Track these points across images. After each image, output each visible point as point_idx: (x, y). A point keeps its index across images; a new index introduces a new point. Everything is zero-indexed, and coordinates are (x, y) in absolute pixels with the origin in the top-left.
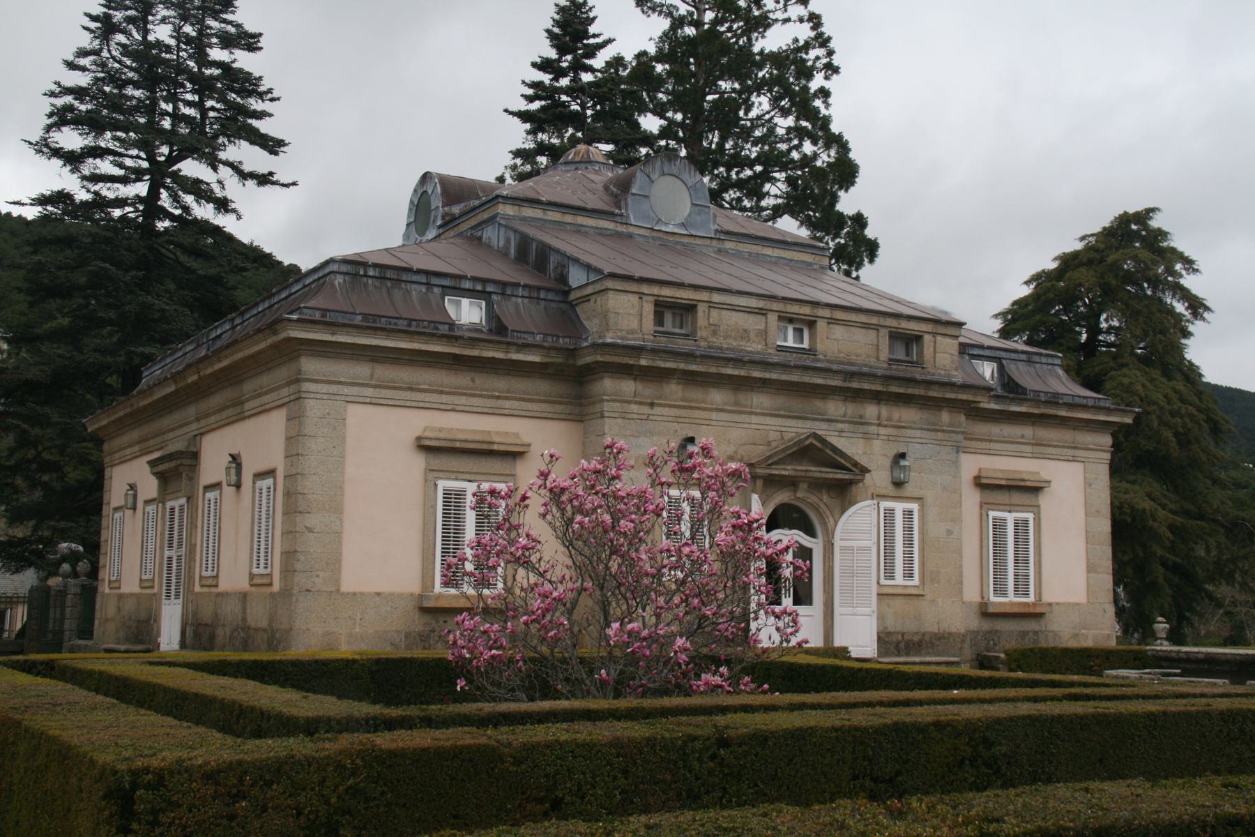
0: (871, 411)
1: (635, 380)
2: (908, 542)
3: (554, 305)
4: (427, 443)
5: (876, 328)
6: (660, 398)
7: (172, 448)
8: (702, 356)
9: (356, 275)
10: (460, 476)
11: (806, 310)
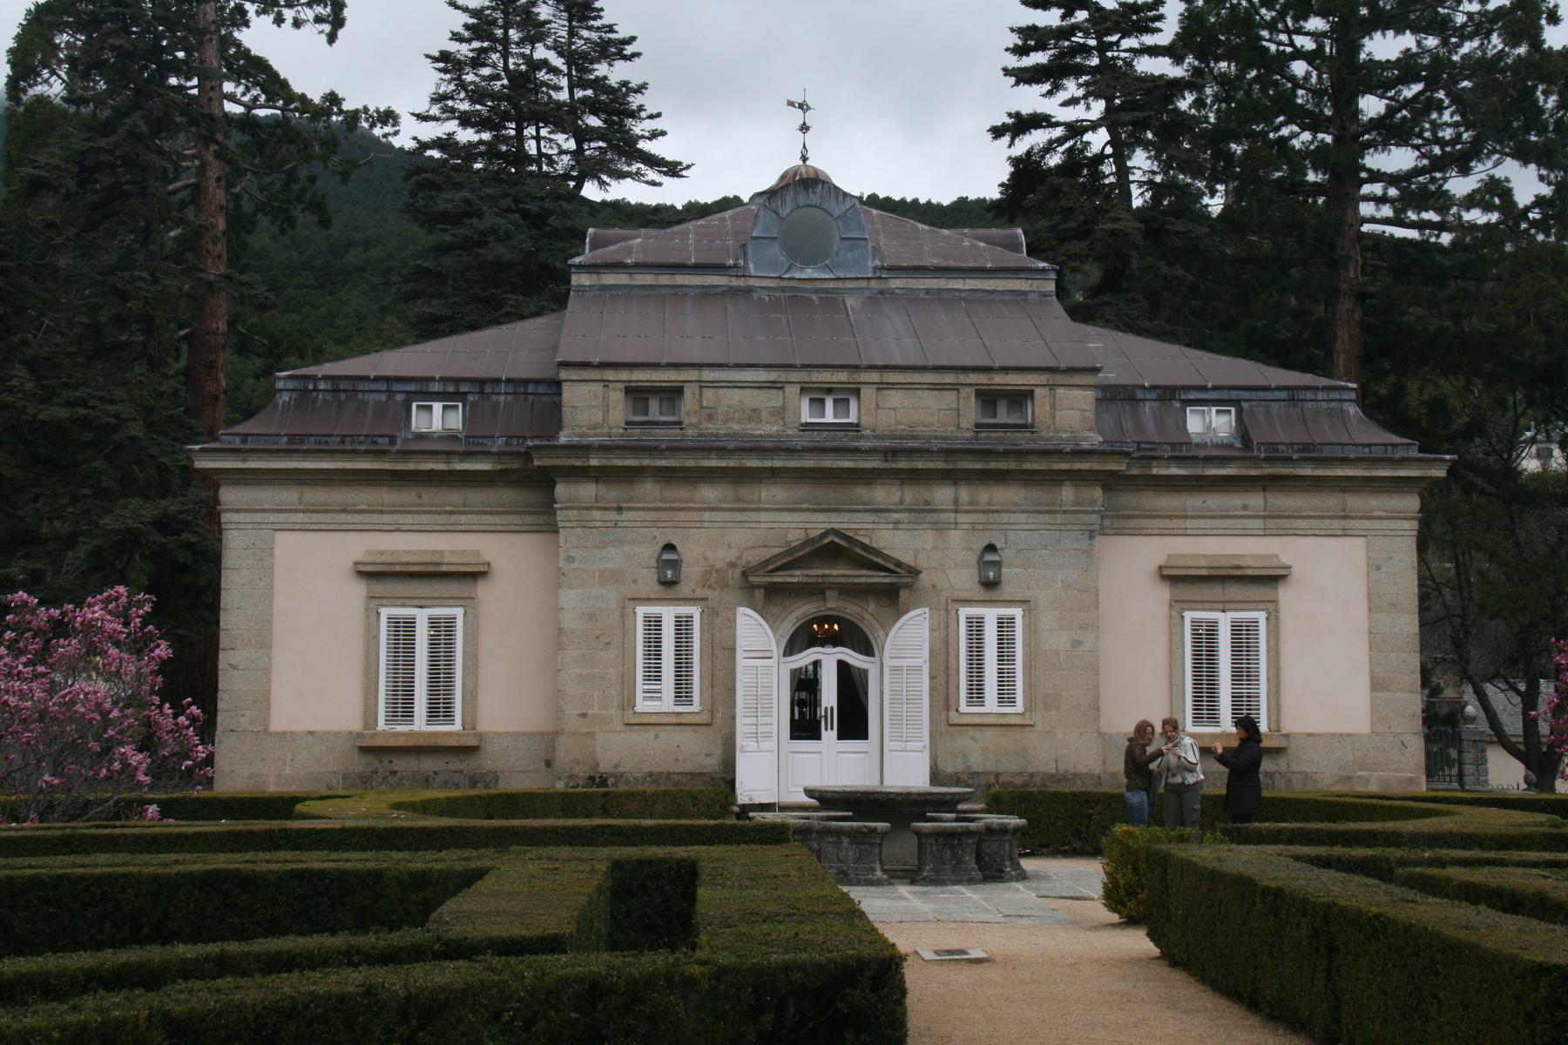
0: (942, 494)
1: (597, 482)
2: (1005, 655)
3: (546, 399)
4: (362, 568)
5: (955, 387)
6: (631, 500)
8: (669, 449)
9: (305, 391)
10: (408, 602)
11: (842, 376)
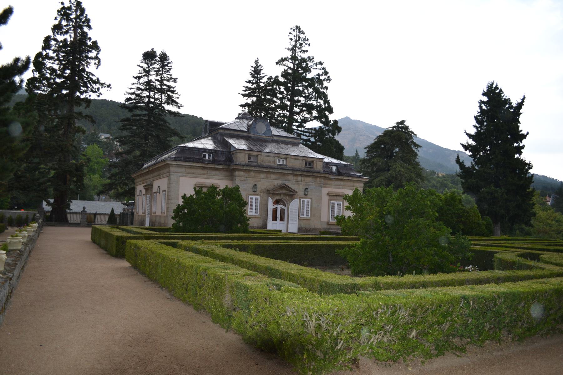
2: (308, 208)
7: (148, 183)
11: (285, 156)
